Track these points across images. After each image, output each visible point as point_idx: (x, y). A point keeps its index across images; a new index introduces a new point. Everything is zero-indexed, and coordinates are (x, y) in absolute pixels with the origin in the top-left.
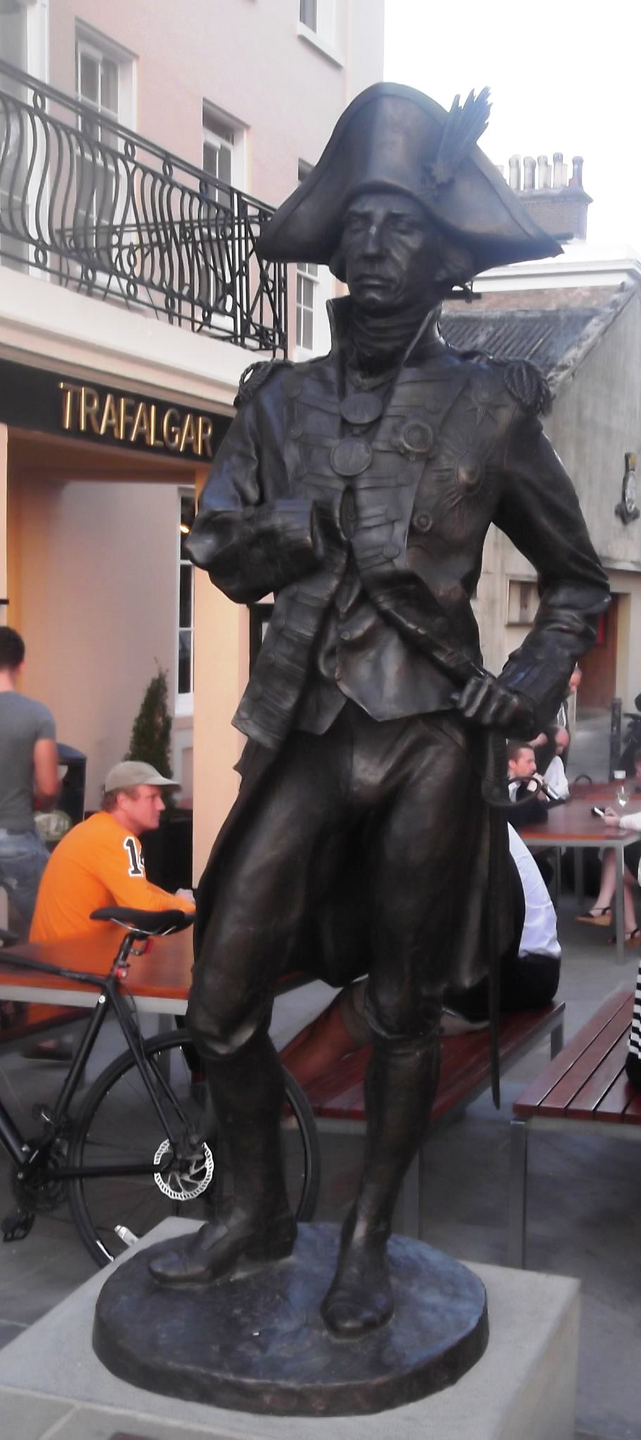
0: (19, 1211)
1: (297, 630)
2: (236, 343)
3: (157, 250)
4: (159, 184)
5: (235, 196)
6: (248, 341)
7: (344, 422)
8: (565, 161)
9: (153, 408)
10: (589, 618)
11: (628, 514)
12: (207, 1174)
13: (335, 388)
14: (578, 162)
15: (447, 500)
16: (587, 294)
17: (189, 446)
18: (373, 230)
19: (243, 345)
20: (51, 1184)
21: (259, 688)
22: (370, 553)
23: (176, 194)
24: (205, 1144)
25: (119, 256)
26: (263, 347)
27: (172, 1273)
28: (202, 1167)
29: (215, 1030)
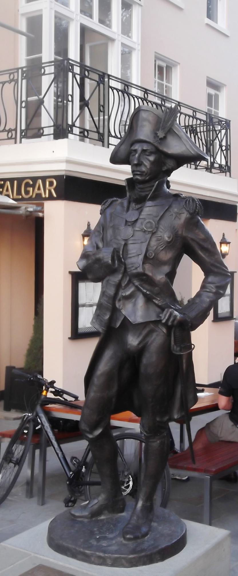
0: (70, 496)
1: (108, 292)
6: (213, 170)
7: (126, 221)
10: (218, 287)
12: (130, 486)
13: (125, 209)
15: (160, 247)
18: (137, 155)
20: (80, 487)
21: (98, 312)
22: (130, 266)
23: (183, 116)
24: (130, 475)
26: (222, 172)
27: (77, 514)
28: (128, 484)
29: (88, 430)
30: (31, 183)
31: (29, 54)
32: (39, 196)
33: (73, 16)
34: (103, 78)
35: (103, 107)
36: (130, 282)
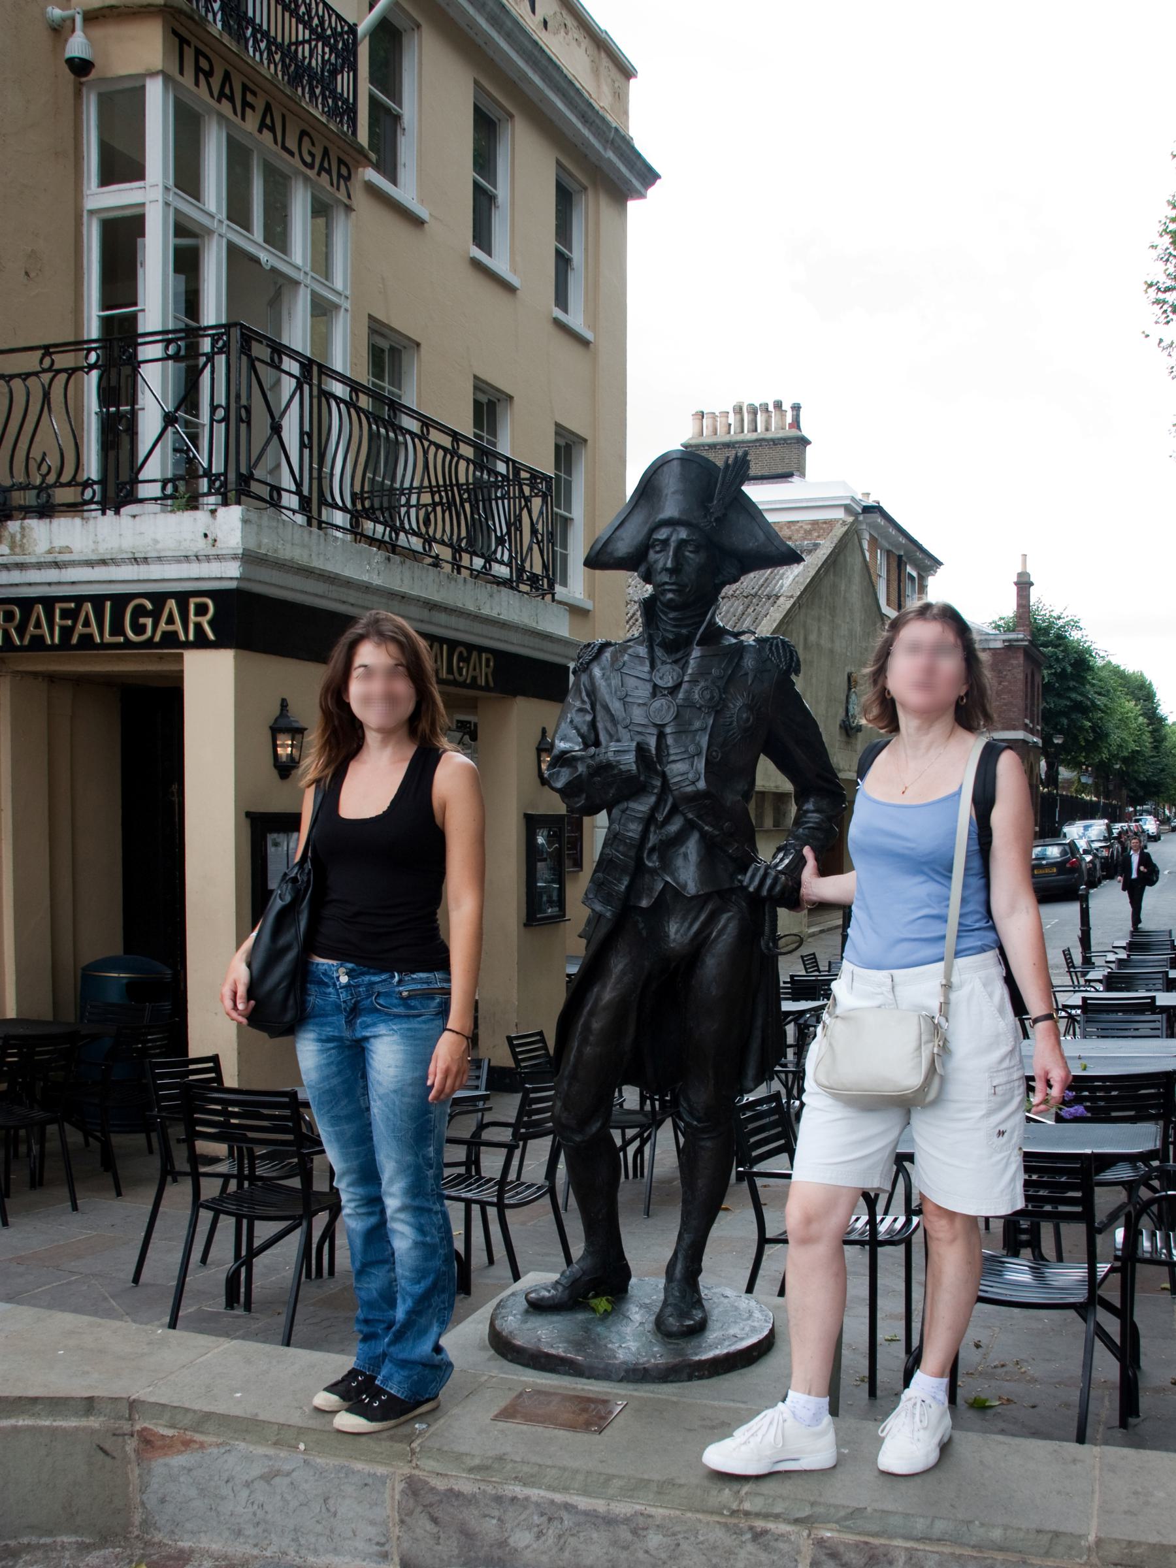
2: (512, 588)
3: (439, 509)
4: (449, 457)
5: (511, 463)
7: (655, 686)
8: (783, 408)
9: (445, 647)
11: (852, 728)
14: (796, 408)
16: (808, 527)
17: (474, 678)
19: (516, 589)
25: (408, 513)
30: (149, 606)
31: (105, 306)
32: (170, 639)
33: (214, 225)
34: (310, 372)
35: (310, 435)
36: (674, 810)
